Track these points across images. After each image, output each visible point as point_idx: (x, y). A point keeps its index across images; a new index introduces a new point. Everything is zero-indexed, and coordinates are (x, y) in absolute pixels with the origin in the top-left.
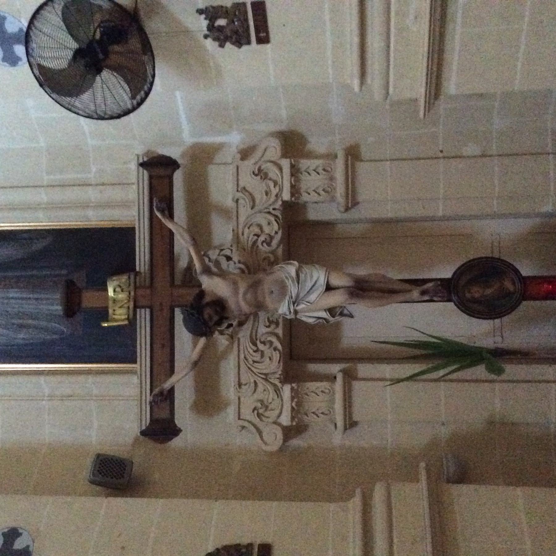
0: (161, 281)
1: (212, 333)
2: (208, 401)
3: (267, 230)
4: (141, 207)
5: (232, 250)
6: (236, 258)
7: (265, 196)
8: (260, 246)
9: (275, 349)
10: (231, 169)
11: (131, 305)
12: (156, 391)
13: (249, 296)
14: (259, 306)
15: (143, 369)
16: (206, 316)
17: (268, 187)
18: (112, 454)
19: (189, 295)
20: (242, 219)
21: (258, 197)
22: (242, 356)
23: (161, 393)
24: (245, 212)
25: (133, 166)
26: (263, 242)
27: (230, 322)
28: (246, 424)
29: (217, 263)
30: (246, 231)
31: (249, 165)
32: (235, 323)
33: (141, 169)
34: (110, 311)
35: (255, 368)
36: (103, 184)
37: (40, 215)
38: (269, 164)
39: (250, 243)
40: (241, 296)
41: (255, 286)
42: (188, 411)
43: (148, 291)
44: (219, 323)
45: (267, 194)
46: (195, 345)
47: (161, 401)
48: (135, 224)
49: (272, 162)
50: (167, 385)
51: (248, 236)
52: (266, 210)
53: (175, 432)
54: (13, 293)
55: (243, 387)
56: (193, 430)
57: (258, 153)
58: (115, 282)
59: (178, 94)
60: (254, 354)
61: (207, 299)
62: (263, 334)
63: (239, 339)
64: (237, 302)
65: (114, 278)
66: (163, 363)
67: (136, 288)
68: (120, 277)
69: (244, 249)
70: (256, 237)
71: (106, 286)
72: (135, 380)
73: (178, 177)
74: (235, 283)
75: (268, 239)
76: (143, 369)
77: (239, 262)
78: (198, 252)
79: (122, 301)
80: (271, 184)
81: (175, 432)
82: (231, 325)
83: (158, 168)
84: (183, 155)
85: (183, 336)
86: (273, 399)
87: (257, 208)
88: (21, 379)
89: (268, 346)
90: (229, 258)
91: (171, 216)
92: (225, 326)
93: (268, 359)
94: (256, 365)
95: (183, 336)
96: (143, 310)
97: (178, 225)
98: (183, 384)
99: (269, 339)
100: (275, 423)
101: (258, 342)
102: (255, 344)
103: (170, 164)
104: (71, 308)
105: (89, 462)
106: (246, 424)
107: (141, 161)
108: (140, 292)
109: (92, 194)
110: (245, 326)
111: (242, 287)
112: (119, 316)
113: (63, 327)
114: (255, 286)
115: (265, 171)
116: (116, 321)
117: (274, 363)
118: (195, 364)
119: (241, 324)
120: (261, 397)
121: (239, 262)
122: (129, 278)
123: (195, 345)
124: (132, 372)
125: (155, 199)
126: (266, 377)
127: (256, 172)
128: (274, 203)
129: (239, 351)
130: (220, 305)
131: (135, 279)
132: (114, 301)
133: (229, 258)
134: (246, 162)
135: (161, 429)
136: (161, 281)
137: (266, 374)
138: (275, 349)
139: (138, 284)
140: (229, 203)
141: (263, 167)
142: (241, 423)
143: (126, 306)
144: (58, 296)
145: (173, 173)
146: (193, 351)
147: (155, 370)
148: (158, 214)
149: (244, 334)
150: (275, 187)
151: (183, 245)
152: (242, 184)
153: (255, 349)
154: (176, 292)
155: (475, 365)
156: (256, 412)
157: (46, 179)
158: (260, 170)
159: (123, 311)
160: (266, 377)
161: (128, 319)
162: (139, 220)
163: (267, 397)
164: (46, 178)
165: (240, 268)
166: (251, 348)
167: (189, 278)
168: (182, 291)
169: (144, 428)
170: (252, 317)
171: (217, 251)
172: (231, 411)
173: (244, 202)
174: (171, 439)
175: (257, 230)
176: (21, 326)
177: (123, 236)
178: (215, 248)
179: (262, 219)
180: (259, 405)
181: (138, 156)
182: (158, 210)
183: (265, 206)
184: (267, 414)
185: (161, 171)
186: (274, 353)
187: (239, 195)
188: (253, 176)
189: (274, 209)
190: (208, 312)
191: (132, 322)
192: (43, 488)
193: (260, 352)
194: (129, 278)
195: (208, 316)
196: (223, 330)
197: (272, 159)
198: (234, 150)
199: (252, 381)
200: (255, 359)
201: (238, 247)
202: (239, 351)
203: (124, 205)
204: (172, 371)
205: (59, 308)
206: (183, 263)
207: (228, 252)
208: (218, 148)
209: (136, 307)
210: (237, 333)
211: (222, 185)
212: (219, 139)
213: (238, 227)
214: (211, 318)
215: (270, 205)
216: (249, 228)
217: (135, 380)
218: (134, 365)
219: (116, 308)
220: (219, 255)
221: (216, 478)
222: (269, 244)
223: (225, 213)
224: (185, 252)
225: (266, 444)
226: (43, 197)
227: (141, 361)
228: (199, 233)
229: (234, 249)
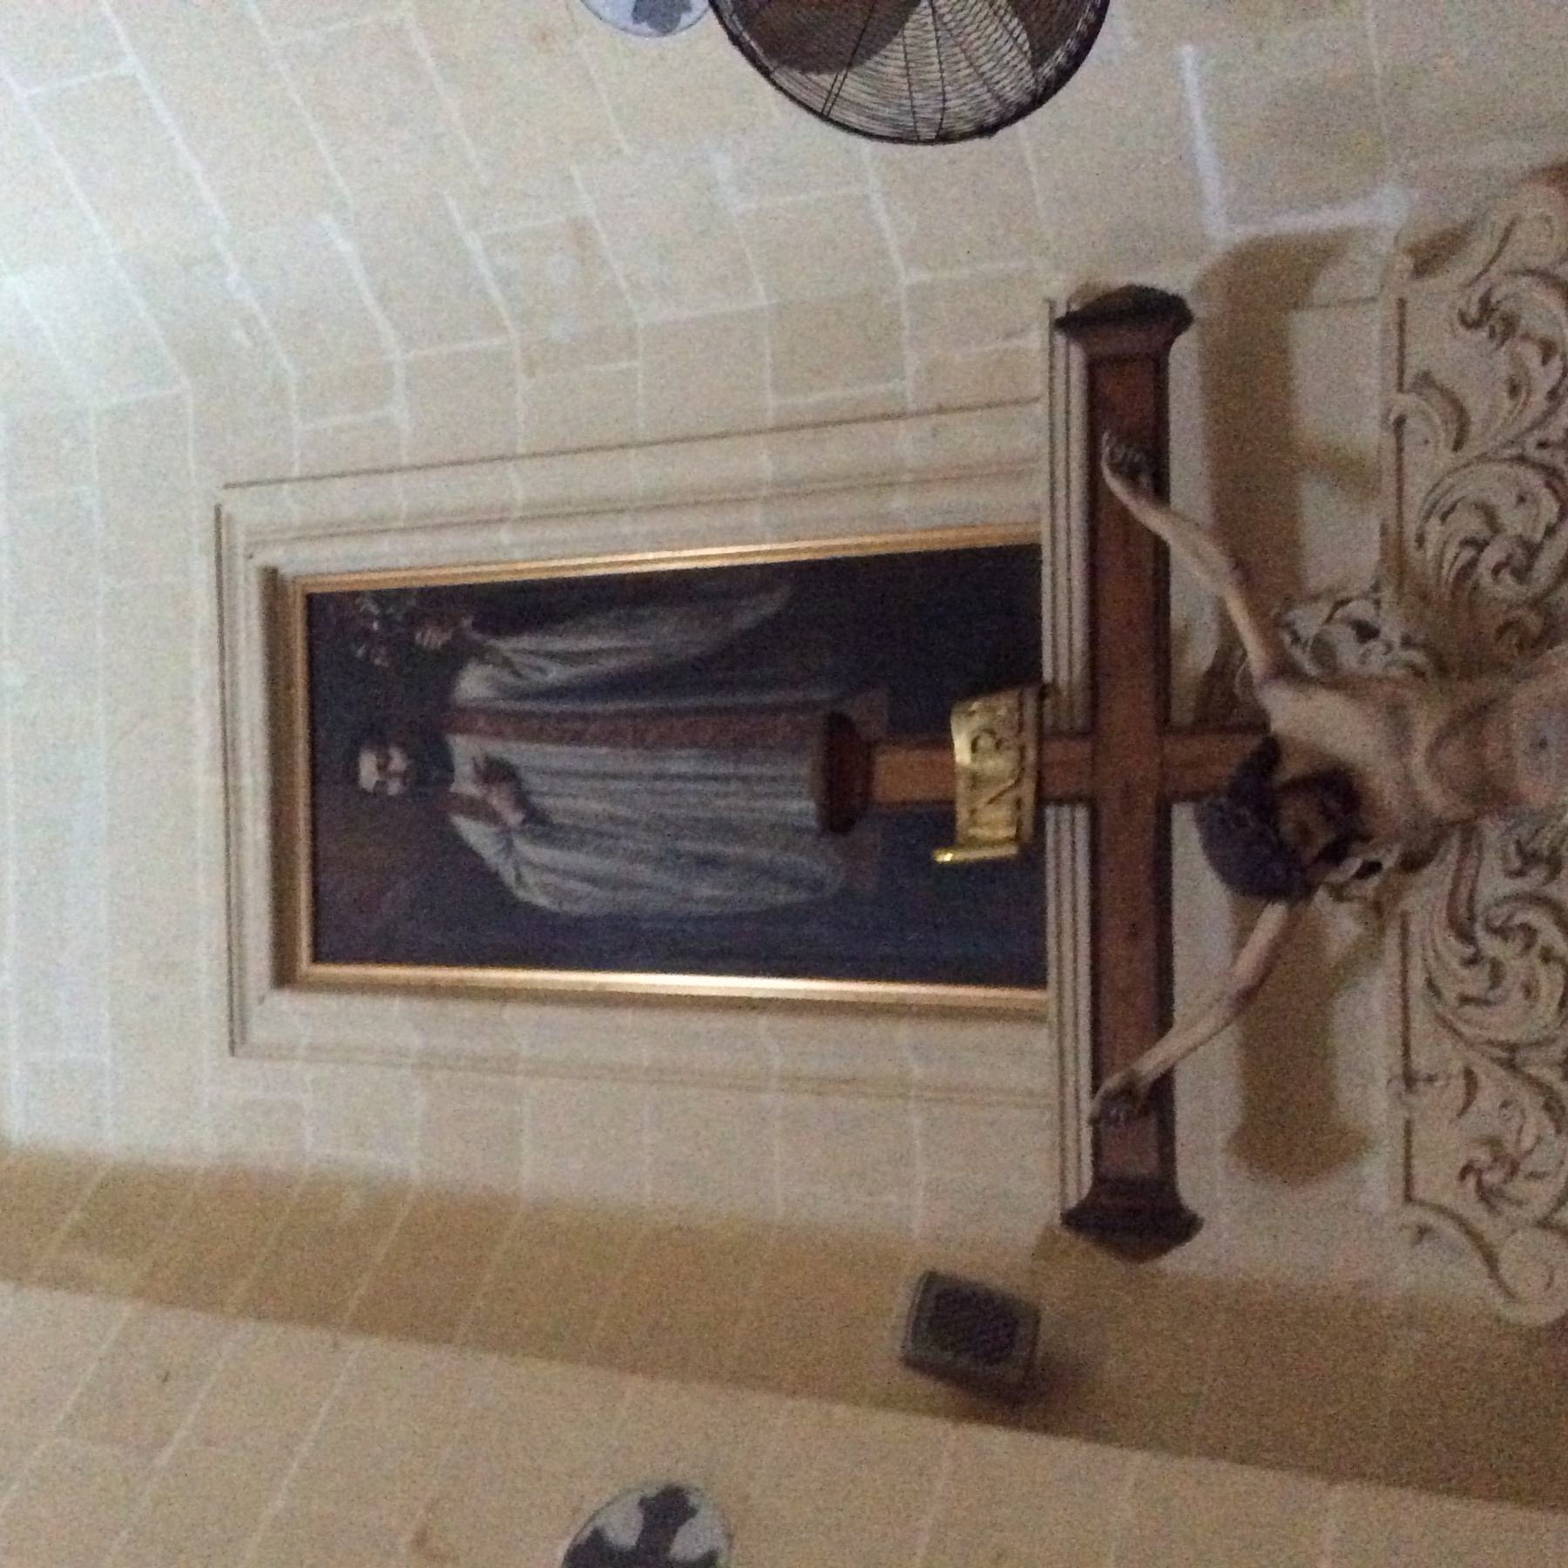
0: (1127, 709)
1: (1308, 890)
2: (1292, 1130)
3: (1514, 521)
4: (1060, 474)
5: (1377, 603)
6: (1392, 630)
7: (1507, 404)
8: (1486, 580)
9: (1547, 956)
10: (1383, 312)
11: (1027, 791)
12: (1112, 1082)
13: (1452, 755)
14: (1490, 794)
15: (1068, 1003)
16: (1287, 828)
17: (1516, 360)
18: (975, 1278)
19: (1225, 758)
20: (1418, 488)
21: (1478, 409)
22: (1417, 979)
23: (1127, 1091)
24: (1429, 460)
25: (1036, 340)
26: (1496, 571)
27: (1373, 857)
28: (1431, 1219)
29: (1323, 650)
30: (1434, 528)
31: (1450, 287)
32: (1389, 862)
33: (1060, 340)
34: (963, 815)
35: (1467, 1022)
36: (941, 410)
37: (755, 516)
38: (1524, 281)
39: (1449, 573)
40: (1417, 760)
41: (1473, 720)
42: (1219, 1159)
43: (1082, 749)
44: (1335, 854)
45: (1514, 390)
46: (1243, 933)
47: (1128, 1119)
48: (1039, 533)
49: (1530, 272)
50: (1150, 1064)
51: (1439, 550)
52: (1508, 453)
53: (1175, 1225)
54: (682, 763)
55: (1421, 1086)
56: (1239, 1227)
57: (1482, 248)
58: (977, 717)
59: (1187, 53)
60: (1465, 973)
61: (1292, 768)
62: (1498, 904)
63: (1404, 916)
64: (1408, 779)
65: (975, 706)
66: (1135, 991)
67: (1041, 740)
68: (993, 701)
69: (1424, 597)
70: (1468, 554)
71: (949, 731)
72: (1041, 1040)
73: (1185, 357)
74: (1396, 713)
75: (1519, 553)
76: (1068, 1003)
77: (1407, 642)
78: (1256, 610)
79: (1001, 780)
80: (1532, 355)
81: (1175, 1225)
82: (1371, 868)
83: (1120, 335)
84: (1201, 288)
85: (1200, 891)
86: (1539, 1139)
87: (1471, 450)
88: (698, 1022)
89: (1517, 945)
90: (1366, 632)
91: (1160, 492)
92: (1353, 871)
93: (1517, 995)
94: (1470, 1011)
95: (1200, 891)
96: (1065, 812)
97: (1184, 525)
98: (1203, 1064)
99: (1519, 918)
100: (1544, 1224)
101: (1480, 933)
102: (1466, 936)
103: (1157, 313)
104: (844, 804)
105: (901, 1302)
106: (1431, 1219)
107: (1061, 312)
108: (1055, 750)
109: (907, 445)
110: (1429, 871)
111: (1424, 726)
112: (989, 830)
113: (820, 864)
114: (1473, 720)
115: (1507, 307)
116: (973, 842)
117: (1541, 1007)
118: (1247, 997)
119: (1412, 864)
120: (1492, 1126)
121: (1407, 642)
122: (1021, 705)
123: (1243, 933)
124: (1034, 1017)
125: (1105, 437)
126: (1511, 1058)
127: (1474, 311)
128: (1538, 424)
129: (1405, 957)
130: (1338, 788)
131: (1040, 708)
132: (976, 780)
133: (1366, 632)
134: (1431, 283)
135: (1132, 1211)
136: (1127, 709)
137: (1513, 1048)
138: (1547, 956)
139: (1048, 721)
140: (1369, 435)
141: (1497, 296)
142: (1415, 1215)
143: (1010, 796)
144: (804, 771)
145: (1169, 343)
146: (1241, 940)
147: (1106, 1020)
148: (1115, 485)
149: (1425, 899)
150: (1544, 362)
151: (1201, 587)
152: (1414, 364)
153: (1469, 951)
154: (1179, 750)
155: (1173, 1121)
156: (1471, 1181)
157: (771, 404)
158: (1486, 306)
159: (1002, 813)
160: (1511, 1058)
161: (1017, 839)
162: (1053, 507)
163: (1514, 1125)
164: (771, 401)
165: (1411, 666)
166: (1453, 950)
167: (1225, 702)
168: (1196, 747)
169: (1073, 1203)
170: (1455, 841)
171: (1324, 608)
172: (1376, 1175)
173: (1429, 419)
174: (1163, 1250)
175: (1473, 525)
176: (707, 862)
177: (1006, 572)
178: (1315, 598)
179: (1492, 483)
180: (1483, 1156)
181: (1052, 305)
182: (1116, 469)
183: (1511, 433)
184: (1519, 1187)
185: (1128, 340)
186: (1542, 972)
187: (1407, 401)
188: (1461, 331)
189: (1542, 445)
190: (1294, 813)
191: (1031, 852)
192: (750, 1372)
193: (1488, 967)
194: (1021, 705)
195: (1296, 829)
196: (1343, 886)
197: (1534, 262)
198: (1384, 247)
199: (1456, 1066)
200: (1472, 990)
201: (1400, 585)
202: (1405, 957)
203: (1010, 471)
204: (1164, 1023)
205: (810, 805)
206: (1198, 656)
207: (1360, 609)
208: (1322, 252)
209: (1041, 800)
210: (1397, 896)
211: (1341, 380)
212: (1325, 220)
213: (1400, 515)
214: (1305, 833)
215: (1530, 429)
216: (1444, 518)
217: (1041, 1040)
218: (1034, 995)
219: (981, 804)
220: (1330, 619)
221: (1319, 1399)
222: (1522, 574)
223: (1351, 475)
224: (1208, 616)
225: (1510, 1295)
226: (762, 462)
227: (1060, 983)
228: (1260, 549)
229: (1387, 593)
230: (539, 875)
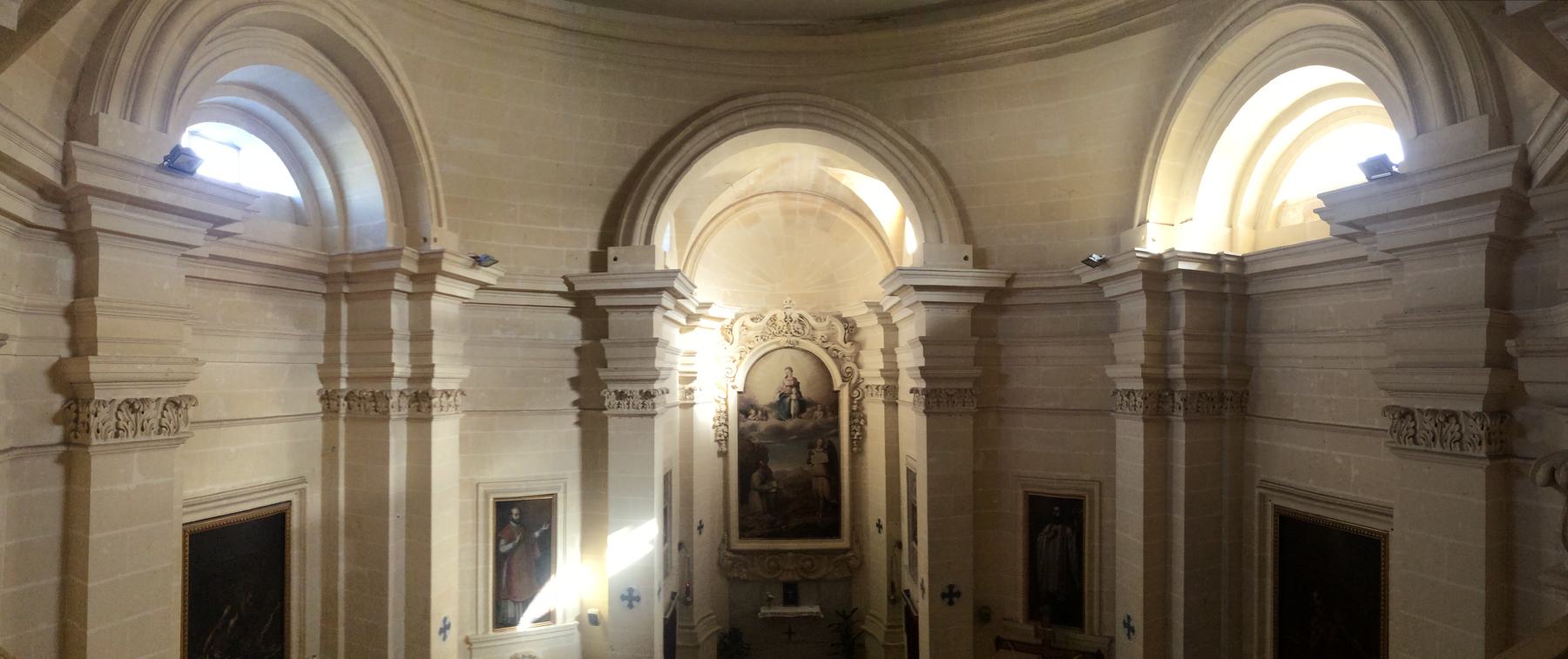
230: (1042, 538)
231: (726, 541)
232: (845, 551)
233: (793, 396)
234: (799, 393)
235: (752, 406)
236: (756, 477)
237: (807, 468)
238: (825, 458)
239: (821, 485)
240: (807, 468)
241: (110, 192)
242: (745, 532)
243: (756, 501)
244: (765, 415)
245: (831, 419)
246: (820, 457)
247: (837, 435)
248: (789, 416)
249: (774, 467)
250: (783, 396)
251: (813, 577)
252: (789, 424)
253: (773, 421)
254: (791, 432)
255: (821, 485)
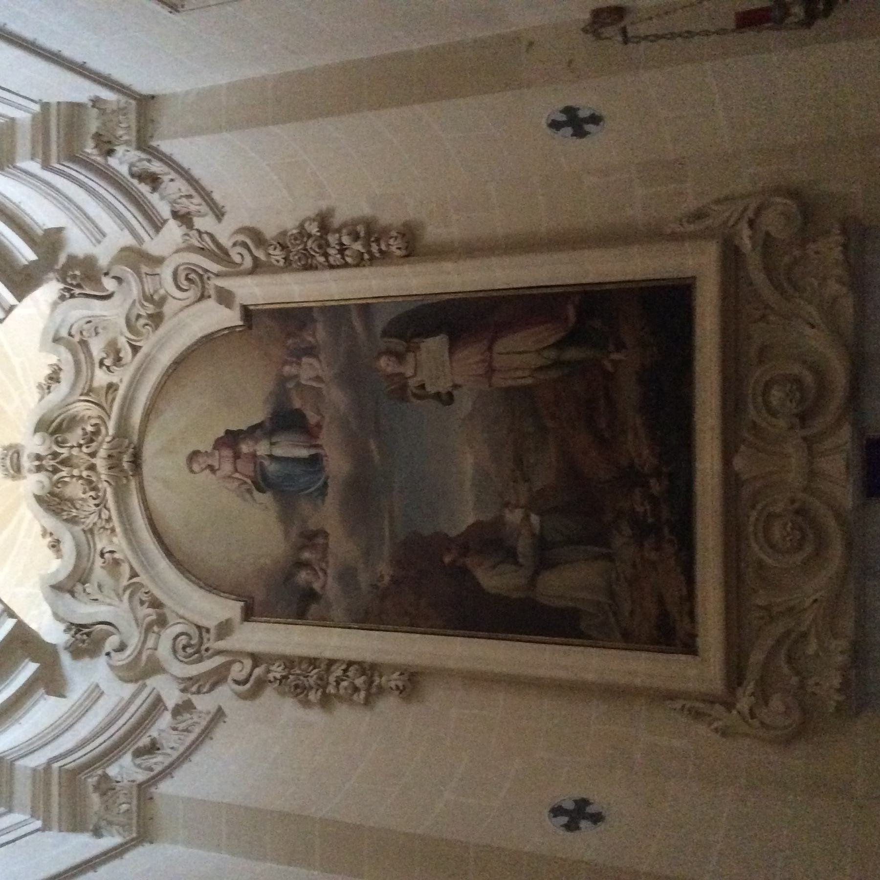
231: (696, 707)
232: (731, 258)
233: (262, 449)
234: (253, 431)
235: (288, 577)
236: (494, 579)
237: (465, 403)
238: (435, 346)
239: (521, 353)
240: (465, 403)
241: (94, 81)
242: (671, 633)
243: (570, 582)
244: (312, 538)
245: (320, 334)
246: (433, 361)
247: (366, 309)
248: (315, 462)
249: (465, 515)
250: (262, 482)
251: (839, 378)
252: (337, 465)
253: (328, 515)
254: (360, 458)
255: (521, 353)
